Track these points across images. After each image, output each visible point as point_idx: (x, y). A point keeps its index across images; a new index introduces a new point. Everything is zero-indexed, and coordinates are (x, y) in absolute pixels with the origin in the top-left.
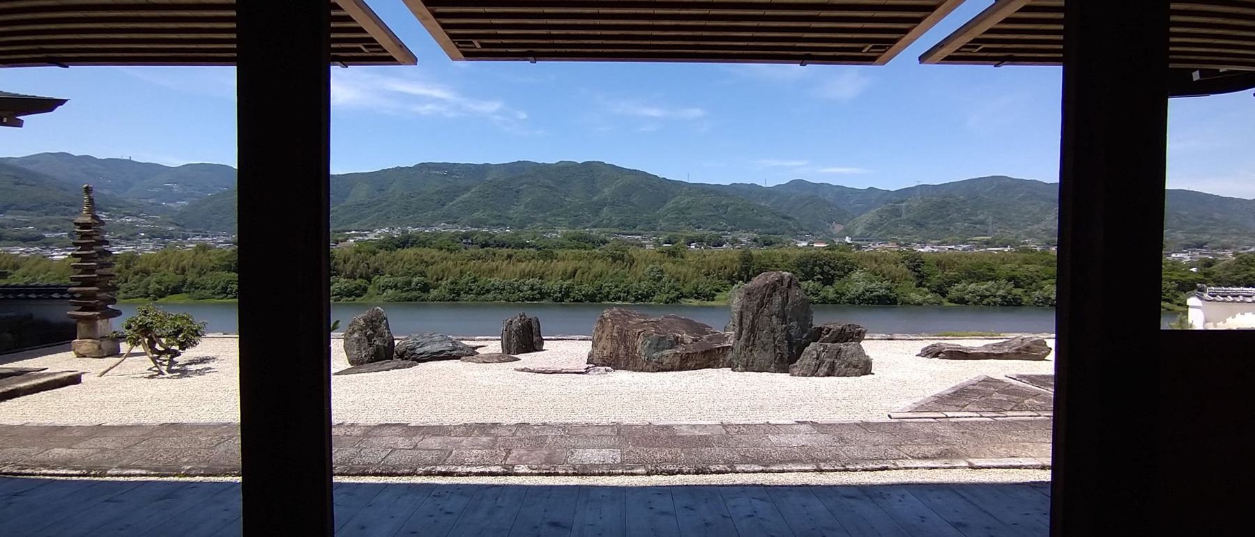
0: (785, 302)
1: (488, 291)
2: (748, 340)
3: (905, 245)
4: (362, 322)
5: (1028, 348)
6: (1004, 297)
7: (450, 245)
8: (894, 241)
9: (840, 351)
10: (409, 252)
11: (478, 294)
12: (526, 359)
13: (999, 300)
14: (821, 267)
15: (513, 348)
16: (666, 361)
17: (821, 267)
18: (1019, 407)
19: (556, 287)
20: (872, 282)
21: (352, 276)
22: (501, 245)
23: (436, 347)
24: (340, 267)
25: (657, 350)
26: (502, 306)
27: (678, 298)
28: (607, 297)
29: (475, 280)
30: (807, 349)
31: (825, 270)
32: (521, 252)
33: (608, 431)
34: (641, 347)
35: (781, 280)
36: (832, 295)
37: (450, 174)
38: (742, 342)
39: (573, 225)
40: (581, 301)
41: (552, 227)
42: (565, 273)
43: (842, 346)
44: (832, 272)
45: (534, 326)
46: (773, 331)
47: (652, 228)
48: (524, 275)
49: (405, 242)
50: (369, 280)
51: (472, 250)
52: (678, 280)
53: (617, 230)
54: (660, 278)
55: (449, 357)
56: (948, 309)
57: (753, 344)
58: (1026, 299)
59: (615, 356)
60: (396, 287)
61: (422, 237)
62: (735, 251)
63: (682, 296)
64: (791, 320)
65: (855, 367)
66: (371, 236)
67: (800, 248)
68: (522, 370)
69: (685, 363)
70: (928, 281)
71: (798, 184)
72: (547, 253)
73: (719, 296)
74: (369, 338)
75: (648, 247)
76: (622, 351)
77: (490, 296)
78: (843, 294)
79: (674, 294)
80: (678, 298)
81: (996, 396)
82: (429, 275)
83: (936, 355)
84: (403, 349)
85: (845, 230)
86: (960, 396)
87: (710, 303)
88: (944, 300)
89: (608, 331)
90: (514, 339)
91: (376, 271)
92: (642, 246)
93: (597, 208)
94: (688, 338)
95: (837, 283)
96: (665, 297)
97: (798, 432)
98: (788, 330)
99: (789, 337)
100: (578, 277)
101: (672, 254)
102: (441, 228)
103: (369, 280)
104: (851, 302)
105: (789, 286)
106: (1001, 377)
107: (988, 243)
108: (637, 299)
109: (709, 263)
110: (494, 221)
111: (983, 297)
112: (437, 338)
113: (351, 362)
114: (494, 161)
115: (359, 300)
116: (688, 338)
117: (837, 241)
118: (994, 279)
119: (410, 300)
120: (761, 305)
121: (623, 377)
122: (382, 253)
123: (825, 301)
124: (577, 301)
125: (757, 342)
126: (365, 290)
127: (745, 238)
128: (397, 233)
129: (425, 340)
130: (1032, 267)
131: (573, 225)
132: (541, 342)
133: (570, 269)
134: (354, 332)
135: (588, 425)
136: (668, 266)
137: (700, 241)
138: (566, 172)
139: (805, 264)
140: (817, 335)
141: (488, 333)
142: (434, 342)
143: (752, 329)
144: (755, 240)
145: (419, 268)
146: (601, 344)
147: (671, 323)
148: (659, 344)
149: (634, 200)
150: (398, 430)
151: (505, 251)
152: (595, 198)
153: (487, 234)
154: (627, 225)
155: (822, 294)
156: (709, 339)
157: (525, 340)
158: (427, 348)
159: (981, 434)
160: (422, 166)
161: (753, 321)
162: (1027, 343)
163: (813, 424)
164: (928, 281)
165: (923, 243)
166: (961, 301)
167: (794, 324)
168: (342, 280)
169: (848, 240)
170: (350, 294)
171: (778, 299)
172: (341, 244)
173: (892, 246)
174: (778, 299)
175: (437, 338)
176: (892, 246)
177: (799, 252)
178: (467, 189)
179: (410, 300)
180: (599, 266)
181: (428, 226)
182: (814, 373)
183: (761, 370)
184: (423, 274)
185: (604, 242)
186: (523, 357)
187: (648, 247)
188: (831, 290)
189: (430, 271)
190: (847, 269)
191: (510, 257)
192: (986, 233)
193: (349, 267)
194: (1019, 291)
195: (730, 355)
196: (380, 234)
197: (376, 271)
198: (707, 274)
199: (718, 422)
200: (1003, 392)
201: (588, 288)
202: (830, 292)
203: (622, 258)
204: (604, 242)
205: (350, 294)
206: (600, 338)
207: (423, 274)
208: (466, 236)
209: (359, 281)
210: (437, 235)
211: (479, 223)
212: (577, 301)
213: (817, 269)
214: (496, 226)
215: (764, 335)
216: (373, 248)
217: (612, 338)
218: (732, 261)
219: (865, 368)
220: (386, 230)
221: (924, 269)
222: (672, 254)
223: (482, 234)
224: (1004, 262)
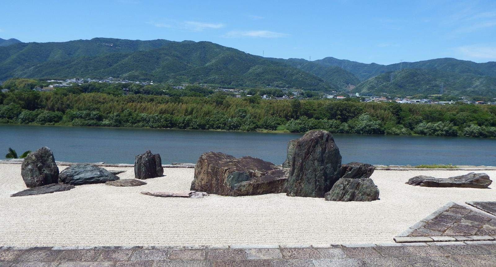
0: (323, 151)
1: (139, 121)
2: (298, 176)
3: (391, 99)
4: (34, 158)
5: (477, 181)
6: (447, 131)
7: (117, 90)
8: (384, 96)
9: (359, 184)
10: (86, 96)
11: (133, 123)
12: (152, 184)
13: (444, 133)
14: (341, 111)
15: (143, 175)
16: (243, 189)
17: (341, 111)
18: (480, 232)
19: (181, 120)
20: (370, 121)
21: (52, 109)
22: (147, 92)
23: (88, 175)
24: (44, 103)
25: (238, 181)
26: (147, 130)
27: (255, 128)
28: (212, 126)
29: (130, 114)
30: (338, 182)
31: (344, 113)
32: (159, 97)
33: (198, 256)
34: (227, 180)
35: (322, 136)
36: (347, 128)
37: (115, 46)
38: (294, 178)
39: (192, 81)
40: (196, 129)
41: (179, 82)
42: (186, 111)
43: (360, 180)
44: (347, 114)
45: (157, 160)
46: (315, 170)
47: (240, 85)
48: (162, 112)
49: (85, 89)
50: (64, 112)
51: (129, 95)
52: (255, 117)
53: (219, 86)
54: (244, 116)
55: (97, 181)
56: (414, 138)
57: (302, 179)
58: (459, 132)
59: (211, 182)
60: (81, 117)
61: (97, 86)
62: (290, 100)
63: (257, 127)
64: (327, 163)
65: (368, 195)
66: (64, 84)
67: (329, 99)
68: (146, 194)
69: (256, 191)
70: (404, 121)
71: (330, 60)
72: (176, 98)
73: (279, 127)
74: (40, 169)
75: (238, 96)
76: (214, 182)
77: (141, 124)
78: (353, 128)
79: (252, 126)
80: (255, 128)
81: (464, 222)
82: (102, 110)
83: (418, 184)
84: (64, 176)
85: (357, 88)
86: (439, 221)
87: (274, 132)
88: (412, 132)
89: (205, 168)
90: (143, 169)
91: (68, 106)
92: (234, 96)
93: (207, 71)
94: (258, 173)
95: (350, 121)
96: (247, 127)
97: (333, 256)
98: (324, 170)
99: (325, 174)
100: (194, 114)
101: (252, 101)
102: (110, 80)
103: (64, 112)
104: (358, 132)
105: (327, 140)
106: (462, 203)
107: (440, 99)
108: (230, 128)
109: (274, 108)
110: (142, 77)
111: (435, 130)
112: (89, 168)
113: (28, 186)
114: (143, 38)
115: (56, 124)
116: (258, 173)
117: (351, 95)
118: (443, 120)
119: (90, 125)
120: (308, 153)
121: (214, 200)
122: (71, 95)
123: (342, 131)
124: (194, 128)
125: (304, 177)
126: (61, 118)
127: (296, 93)
128: (81, 82)
129: (82, 170)
130: (465, 114)
131: (192, 81)
132: (162, 171)
133: (189, 109)
134: (28, 164)
135: (185, 249)
136: (250, 109)
137: (269, 93)
138: (188, 47)
139: (332, 109)
140: (343, 172)
141: (125, 160)
142: (87, 171)
143: (301, 169)
144: (302, 94)
145: (95, 106)
146: (201, 176)
147: (248, 163)
148: (240, 177)
149: (230, 67)
150: (43, 254)
151: (150, 96)
152: (207, 65)
153: (138, 85)
154: (225, 83)
155: (341, 128)
156: (273, 173)
157: (151, 168)
158: (82, 176)
159: (459, 258)
160: (96, 40)
161: (302, 164)
162: (477, 177)
163: (343, 247)
164: (404, 121)
165: (402, 98)
166: (422, 133)
167: (329, 165)
168: (46, 112)
169: (357, 95)
170: (50, 120)
171: (319, 149)
172: (44, 89)
173: (383, 99)
174: (319, 149)
175: (89, 168)
176: (383, 99)
177: (328, 102)
178: (126, 56)
179: (90, 125)
180: (206, 107)
181: (101, 79)
182: (341, 199)
183: (306, 196)
184: (98, 109)
185: (211, 92)
186: (149, 181)
187: (238, 96)
188: (346, 125)
189: (102, 107)
190: (357, 113)
191: (152, 100)
192: (439, 92)
193: (50, 104)
194: (455, 128)
195: (286, 185)
196: (71, 83)
197: (68, 106)
198: (273, 114)
199: (276, 245)
200: (468, 218)
201: (199, 121)
202: (345, 126)
203: (221, 103)
204: (211, 92)
205: (50, 120)
206: (199, 173)
207: (98, 109)
208: (125, 86)
209: (56, 113)
210: (106, 85)
211: (134, 78)
212: (194, 128)
213: (339, 112)
214: (144, 80)
215: (309, 172)
216: (65, 91)
217: (208, 173)
218: (288, 106)
219: (374, 196)
220: (74, 80)
221: (402, 114)
222: (252, 101)
223: (135, 85)
224: (448, 110)
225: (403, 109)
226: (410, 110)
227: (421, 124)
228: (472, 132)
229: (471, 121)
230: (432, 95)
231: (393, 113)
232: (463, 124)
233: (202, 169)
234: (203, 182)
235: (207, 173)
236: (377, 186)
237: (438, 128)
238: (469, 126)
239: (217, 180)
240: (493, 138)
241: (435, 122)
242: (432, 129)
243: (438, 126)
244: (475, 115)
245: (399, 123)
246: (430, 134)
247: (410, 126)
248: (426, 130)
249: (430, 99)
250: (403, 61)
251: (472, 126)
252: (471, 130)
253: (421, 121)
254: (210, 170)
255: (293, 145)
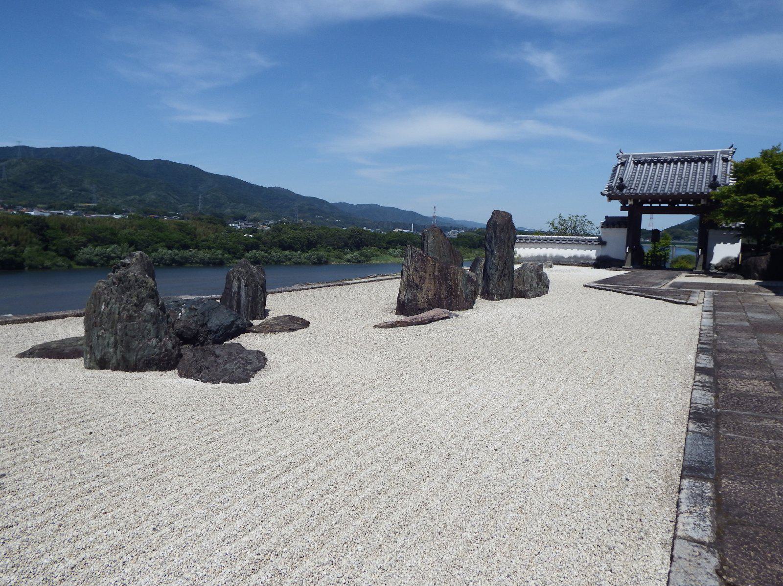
76: (444, 292)
88: (72, 263)
89: (430, 269)
107: (95, 210)
111: (109, 258)
166: (90, 263)
192: (90, 200)
221: (49, 233)
225: (51, 224)
226: (63, 227)
227: (86, 250)
228: (162, 258)
229: (157, 243)
230: (80, 205)
231: (32, 230)
232: (148, 247)
233: (425, 272)
234: (430, 294)
235: (434, 279)
236: (408, 309)
237: (113, 255)
238: (156, 250)
239: (448, 286)
240: (189, 265)
241: (107, 246)
242: (104, 257)
243: (112, 251)
244: (161, 235)
245: (46, 249)
246: (102, 265)
247: (69, 254)
248: (95, 258)
249: (80, 210)
250: (21, 144)
251: (160, 250)
252: (160, 256)
253: (85, 245)
254: (436, 273)
255: (434, 237)
